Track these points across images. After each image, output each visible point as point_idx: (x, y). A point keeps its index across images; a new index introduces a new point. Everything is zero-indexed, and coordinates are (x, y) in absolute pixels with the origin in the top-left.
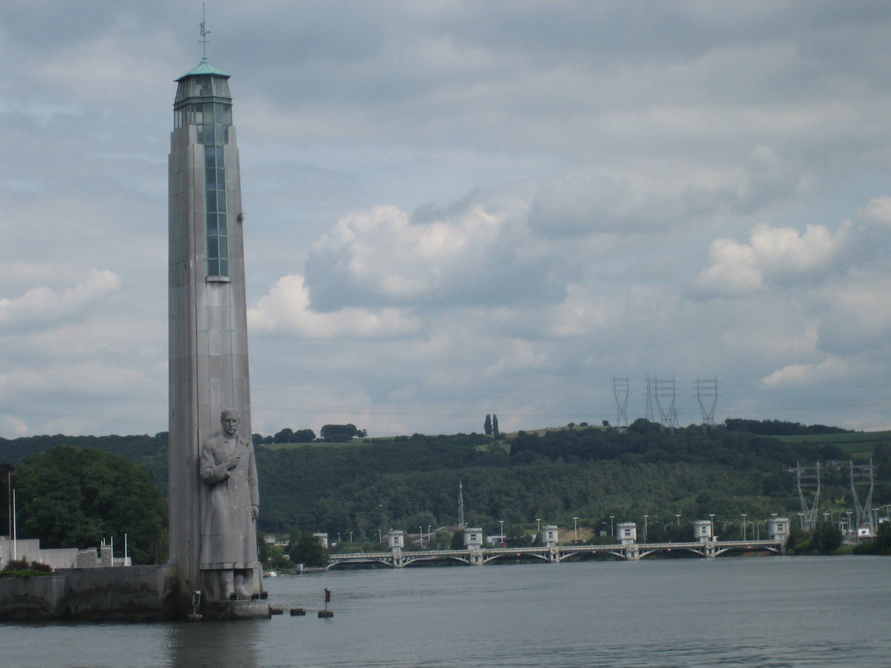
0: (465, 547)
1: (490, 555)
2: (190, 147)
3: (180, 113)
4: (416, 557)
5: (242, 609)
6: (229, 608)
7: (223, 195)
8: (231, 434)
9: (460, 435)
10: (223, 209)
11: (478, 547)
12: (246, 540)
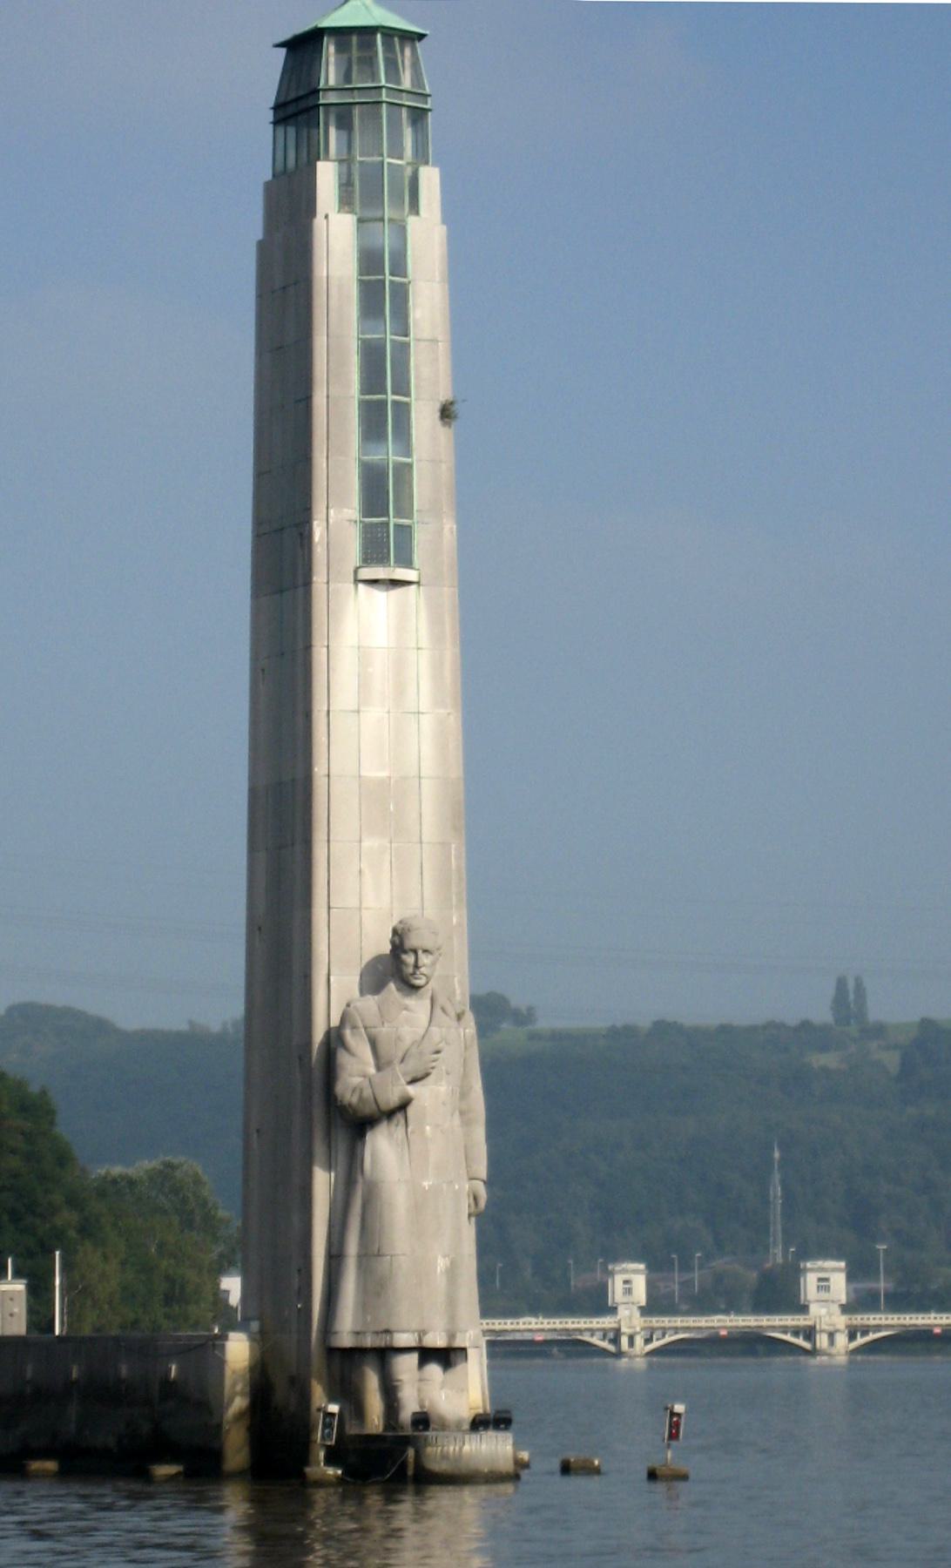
0: (803, 1309)
1: (865, 1331)
2: (319, 222)
3: (291, 131)
4: (676, 1330)
5: (445, 1457)
6: (411, 1452)
7: (403, 350)
8: (416, 988)
9: (771, 1025)
10: (402, 387)
11: (836, 1309)
12: (452, 1272)
